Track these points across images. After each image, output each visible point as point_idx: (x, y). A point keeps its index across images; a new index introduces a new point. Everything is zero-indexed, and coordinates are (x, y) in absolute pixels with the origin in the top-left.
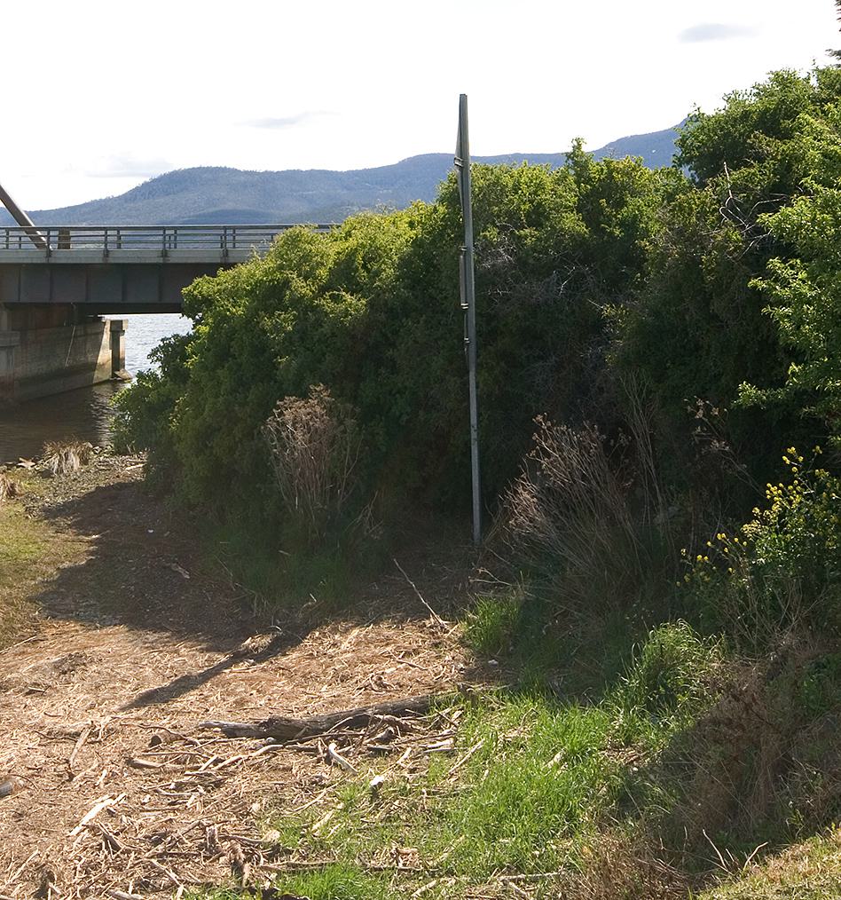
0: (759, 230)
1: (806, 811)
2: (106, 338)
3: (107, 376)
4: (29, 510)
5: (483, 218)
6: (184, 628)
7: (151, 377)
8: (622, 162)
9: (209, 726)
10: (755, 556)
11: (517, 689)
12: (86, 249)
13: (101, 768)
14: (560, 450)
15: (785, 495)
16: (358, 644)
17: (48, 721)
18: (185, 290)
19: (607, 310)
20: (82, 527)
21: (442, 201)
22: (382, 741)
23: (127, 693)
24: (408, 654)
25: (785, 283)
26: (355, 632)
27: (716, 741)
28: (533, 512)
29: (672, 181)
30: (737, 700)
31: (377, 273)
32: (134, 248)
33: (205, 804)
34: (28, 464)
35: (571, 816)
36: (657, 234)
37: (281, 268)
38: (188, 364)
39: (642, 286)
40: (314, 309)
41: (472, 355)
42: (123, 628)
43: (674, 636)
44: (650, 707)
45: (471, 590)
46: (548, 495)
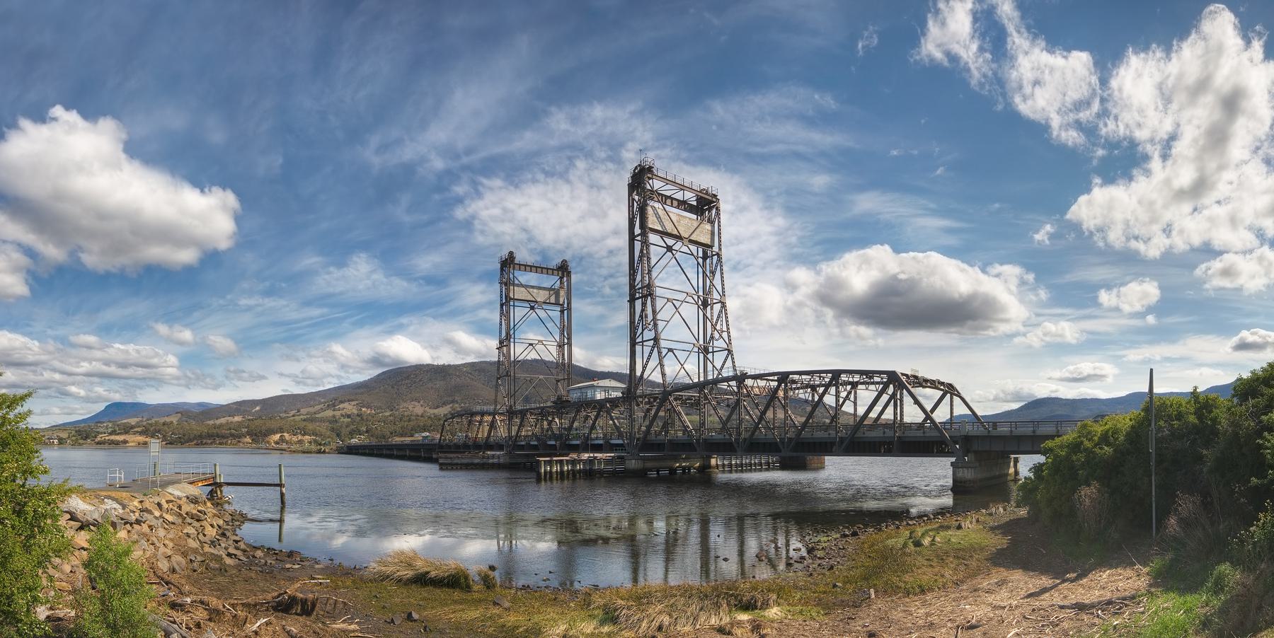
0: (1261, 422)
1: (1266, 621)
2: (1012, 464)
3: (1013, 478)
4: (985, 527)
5: (1158, 417)
6: (1044, 570)
7: (1030, 478)
8: (1212, 396)
9: (1054, 605)
10: (1254, 538)
11: (1168, 589)
12: (1004, 430)
13: (1014, 618)
14: (1186, 504)
15: (1265, 517)
16: (1109, 576)
17: (994, 602)
18: (1042, 446)
19: (1205, 452)
20: (1004, 534)
21: (1142, 410)
22: (1117, 609)
23: (1023, 593)
24: (1128, 579)
25: (1269, 441)
26: (1108, 571)
27: (1238, 602)
28: (1175, 527)
29: (1230, 403)
30: (1245, 587)
31: (1117, 438)
32: (1022, 429)
33: (1052, 632)
34: (984, 511)
35: (1186, 631)
36: (1224, 423)
37: (1079, 437)
38: (1044, 474)
39: (1218, 443)
40: (1093, 452)
41: (1153, 469)
42: (1021, 570)
43: (1225, 568)
44: (1215, 592)
45: (1152, 555)
46: (1181, 521)
